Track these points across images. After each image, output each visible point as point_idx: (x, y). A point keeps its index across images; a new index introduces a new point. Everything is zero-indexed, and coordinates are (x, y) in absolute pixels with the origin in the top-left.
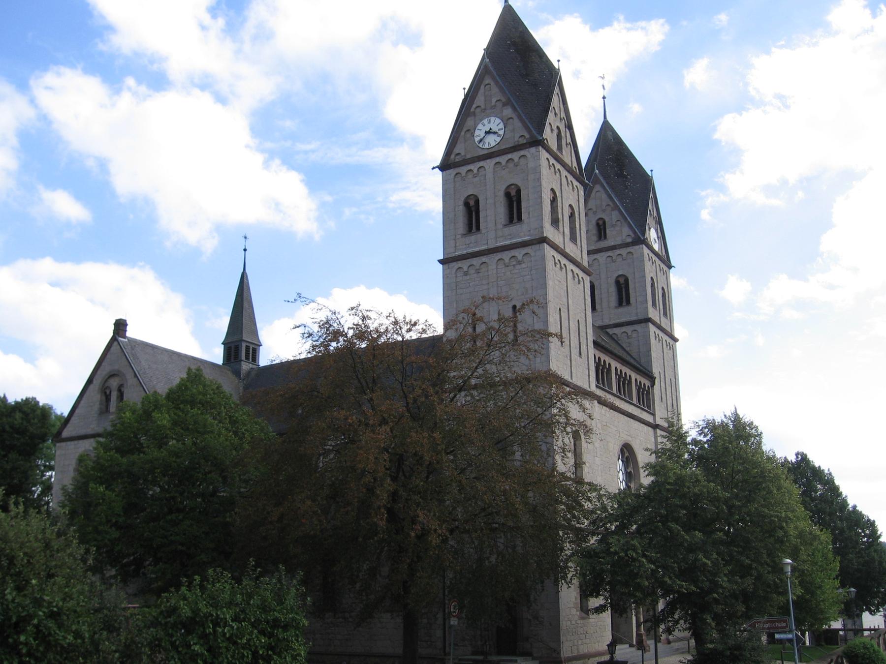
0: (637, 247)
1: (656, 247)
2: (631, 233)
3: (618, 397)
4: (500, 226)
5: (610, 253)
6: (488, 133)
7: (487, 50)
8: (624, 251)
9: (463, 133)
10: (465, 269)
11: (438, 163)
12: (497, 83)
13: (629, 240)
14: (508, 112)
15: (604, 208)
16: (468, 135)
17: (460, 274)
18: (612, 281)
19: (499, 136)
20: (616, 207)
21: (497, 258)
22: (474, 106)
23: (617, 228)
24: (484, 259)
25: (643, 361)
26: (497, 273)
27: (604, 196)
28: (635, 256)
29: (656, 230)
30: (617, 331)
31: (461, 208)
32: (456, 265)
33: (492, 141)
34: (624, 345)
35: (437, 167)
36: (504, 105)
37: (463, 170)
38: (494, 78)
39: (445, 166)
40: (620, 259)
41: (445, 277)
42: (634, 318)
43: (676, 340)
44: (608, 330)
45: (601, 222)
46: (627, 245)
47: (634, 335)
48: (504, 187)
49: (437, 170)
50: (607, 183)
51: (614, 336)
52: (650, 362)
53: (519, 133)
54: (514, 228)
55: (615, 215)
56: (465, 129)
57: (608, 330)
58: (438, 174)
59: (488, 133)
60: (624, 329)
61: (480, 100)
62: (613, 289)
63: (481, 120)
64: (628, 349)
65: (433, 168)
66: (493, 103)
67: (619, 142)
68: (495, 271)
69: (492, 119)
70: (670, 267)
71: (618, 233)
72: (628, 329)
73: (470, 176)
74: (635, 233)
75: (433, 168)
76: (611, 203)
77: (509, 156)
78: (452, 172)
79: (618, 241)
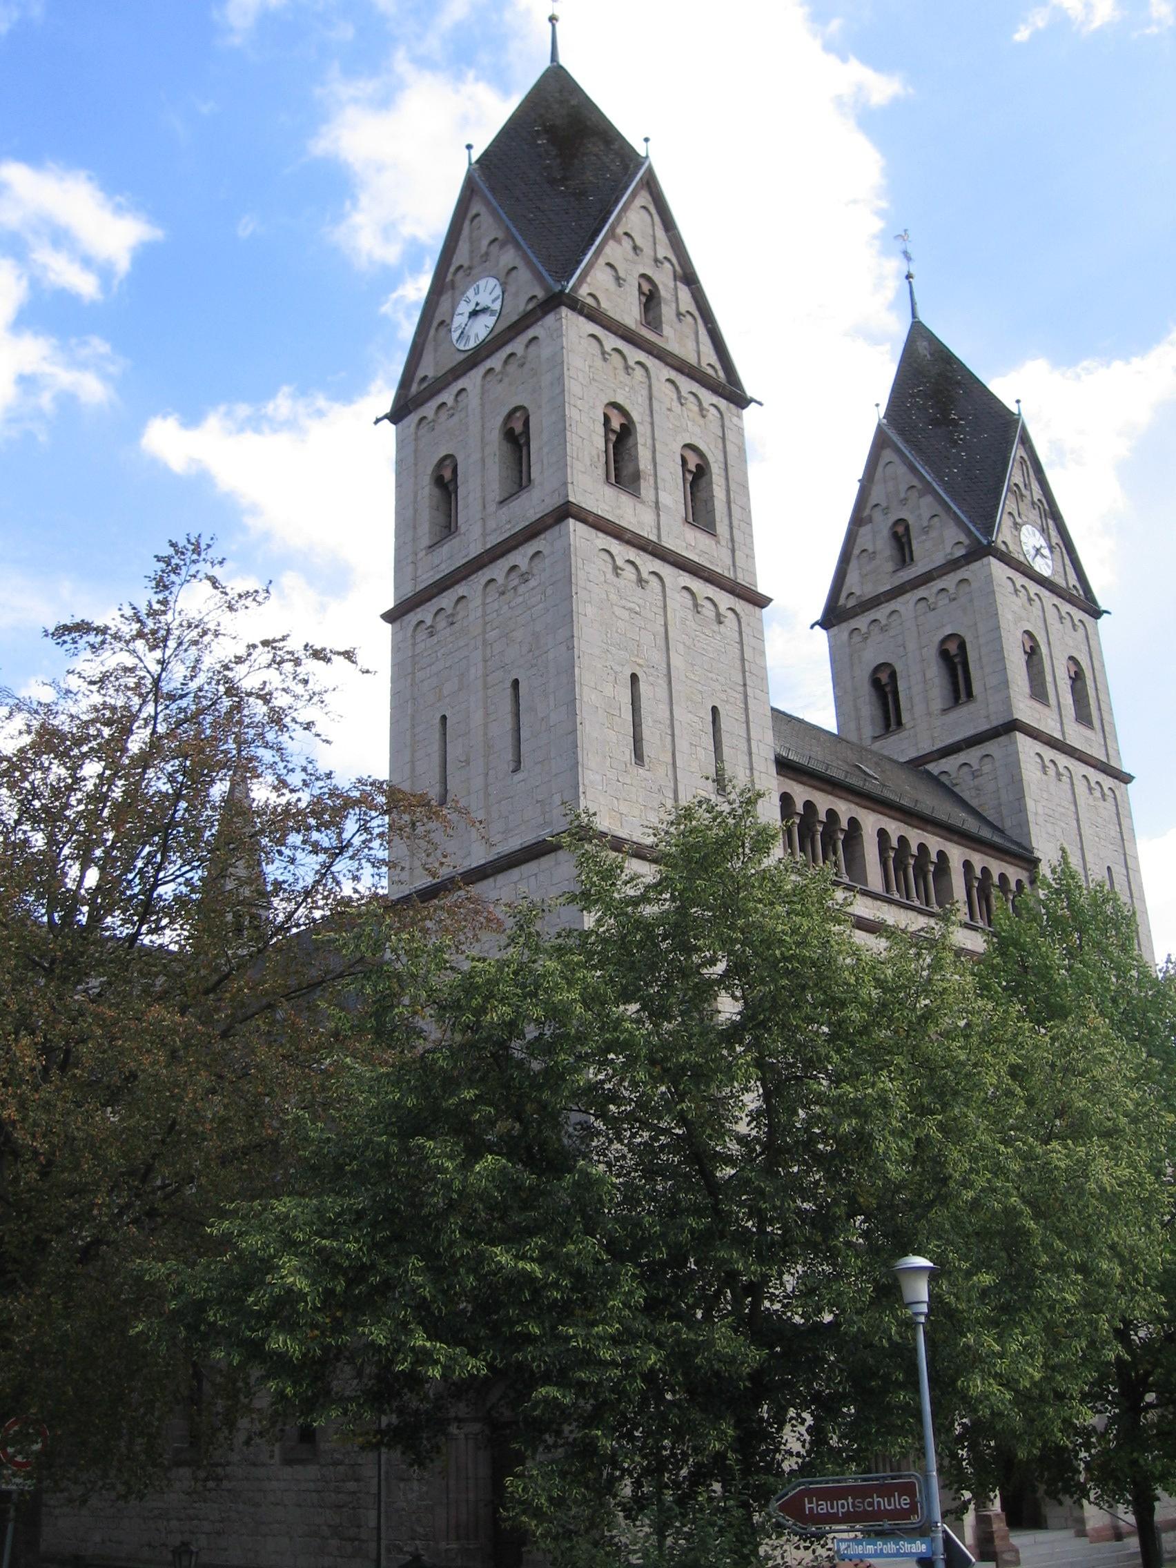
0: (977, 564)
1: (1043, 567)
2: (963, 538)
3: (891, 902)
4: (492, 508)
5: (921, 592)
6: (474, 314)
7: (893, 391)
8: (949, 582)
9: (432, 332)
10: (429, 622)
11: (818, 615)
12: (494, 212)
13: (960, 552)
14: (509, 257)
15: (902, 495)
16: (443, 331)
17: (422, 634)
18: (932, 653)
19: (493, 313)
20: (928, 489)
21: (483, 581)
22: (452, 269)
23: (933, 534)
24: (460, 590)
25: (1008, 824)
26: (484, 615)
27: (902, 470)
28: (975, 585)
29: (1044, 531)
30: (949, 764)
31: (866, 689)
32: (413, 618)
33: (481, 329)
34: (966, 795)
35: (386, 417)
36: (503, 245)
37: (861, 622)
38: (488, 204)
39: (832, 618)
40: (943, 601)
41: (396, 649)
42: (984, 726)
43: (1126, 779)
44: (930, 767)
45: (901, 529)
46: (953, 565)
47: (987, 768)
48: (500, 420)
49: (817, 627)
50: (907, 441)
51: (944, 778)
52: (1024, 824)
53: (528, 288)
54: (964, 711)
55: (927, 505)
56: (435, 324)
57: (930, 767)
58: (821, 634)
59: (474, 314)
60: (962, 757)
61: (462, 256)
62: (935, 672)
63: (463, 293)
64: (974, 803)
65: (378, 421)
66: (484, 249)
67: (944, 357)
68: (479, 613)
69: (482, 283)
70: (1096, 613)
71: (938, 542)
72: (971, 756)
73: (444, 414)
74: (969, 533)
75: (378, 421)
76: (915, 482)
77: (508, 350)
78: (845, 628)
79: (939, 559)
